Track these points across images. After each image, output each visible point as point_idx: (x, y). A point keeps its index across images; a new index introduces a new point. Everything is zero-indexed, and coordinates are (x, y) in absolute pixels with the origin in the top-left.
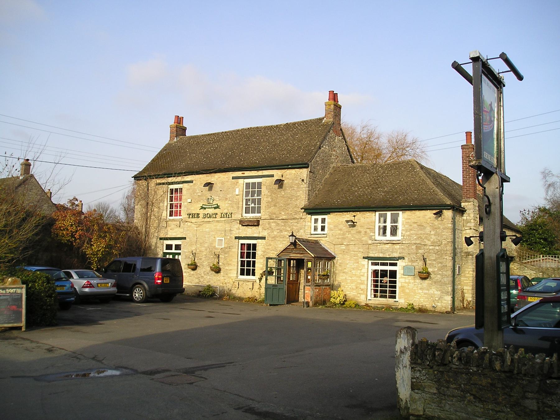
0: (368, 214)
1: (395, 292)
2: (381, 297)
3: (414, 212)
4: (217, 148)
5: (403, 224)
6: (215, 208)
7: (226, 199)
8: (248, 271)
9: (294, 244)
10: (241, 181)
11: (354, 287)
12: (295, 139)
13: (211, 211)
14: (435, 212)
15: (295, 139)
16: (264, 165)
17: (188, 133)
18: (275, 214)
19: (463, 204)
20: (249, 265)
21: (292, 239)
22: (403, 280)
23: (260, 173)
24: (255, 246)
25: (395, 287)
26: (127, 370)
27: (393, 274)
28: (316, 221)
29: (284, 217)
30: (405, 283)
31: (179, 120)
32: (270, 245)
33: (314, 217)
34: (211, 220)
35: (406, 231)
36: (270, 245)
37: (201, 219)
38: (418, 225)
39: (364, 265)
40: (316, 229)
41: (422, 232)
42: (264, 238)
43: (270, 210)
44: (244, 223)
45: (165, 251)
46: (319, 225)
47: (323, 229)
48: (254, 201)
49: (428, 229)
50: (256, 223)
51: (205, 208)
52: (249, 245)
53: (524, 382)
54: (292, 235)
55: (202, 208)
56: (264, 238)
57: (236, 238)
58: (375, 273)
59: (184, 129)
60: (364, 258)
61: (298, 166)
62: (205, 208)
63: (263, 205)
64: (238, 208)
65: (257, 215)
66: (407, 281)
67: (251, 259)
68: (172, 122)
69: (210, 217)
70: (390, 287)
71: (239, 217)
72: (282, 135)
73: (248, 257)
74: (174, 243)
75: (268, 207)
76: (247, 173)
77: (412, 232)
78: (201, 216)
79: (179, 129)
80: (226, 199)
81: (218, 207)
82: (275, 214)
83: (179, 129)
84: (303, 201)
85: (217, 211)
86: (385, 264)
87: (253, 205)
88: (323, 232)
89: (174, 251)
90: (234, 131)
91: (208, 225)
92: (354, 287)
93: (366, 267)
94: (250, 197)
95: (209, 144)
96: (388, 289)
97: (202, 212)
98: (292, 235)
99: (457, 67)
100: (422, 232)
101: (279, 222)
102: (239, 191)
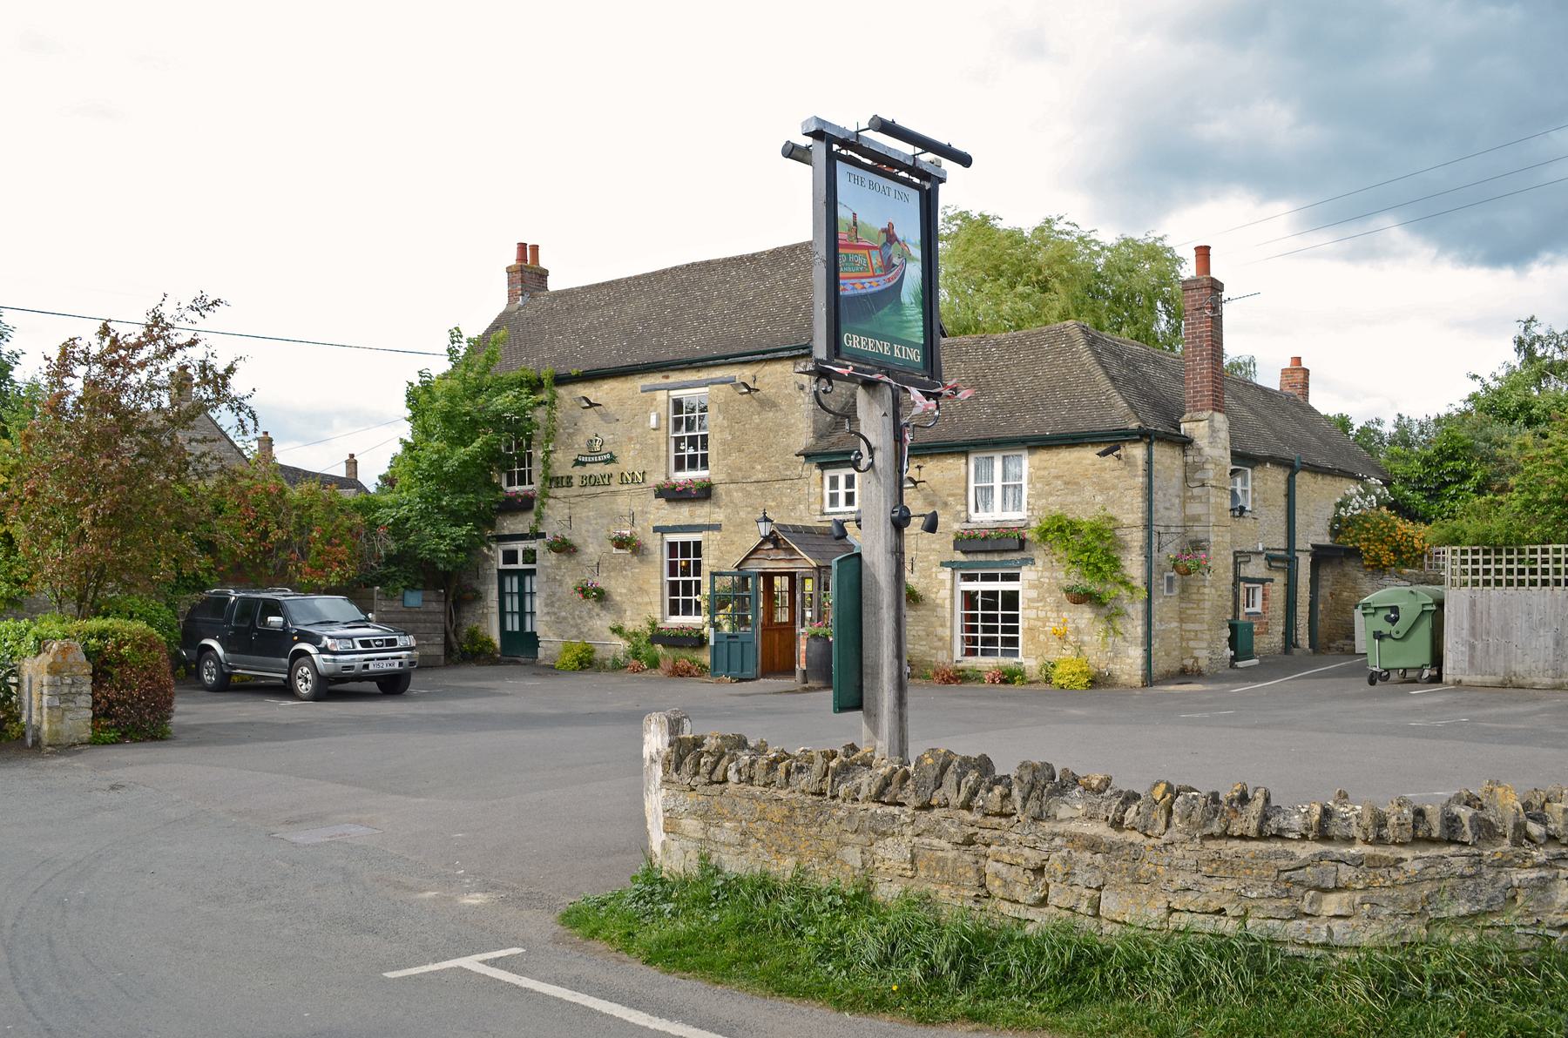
0: (950, 462)
1: (1015, 642)
2: (1004, 653)
3: (1055, 451)
4: (611, 317)
5: (1030, 482)
6: (606, 462)
7: (631, 439)
8: (687, 604)
9: (772, 539)
10: (661, 396)
11: (922, 633)
12: (788, 288)
13: (597, 470)
14: (1102, 449)
15: (788, 288)
16: (709, 355)
17: (554, 284)
18: (740, 469)
19: (1185, 427)
20: (687, 591)
21: (764, 529)
22: (1032, 614)
23: (704, 375)
24: (698, 545)
25: (1016, 630)
26: (293, 839)
27: (1011, 600)
28: (834, 482)
29: (760, 476)
30: (1038, 619)
31: (527, 252)
32: (733, 543)
33: (829, 473)
34: (599, 490)
35: (1039, 496)
36: (733, 543)
37: (575, 490)
38: (1066, 483)
39: (943, 582)
40: (834, 500)
41: (1075, 498)
42: (716, 527)
43: (729, 461)
44: (673, 495)
45: (502, 566)
46: (842, 490)
47: (850, 499)
48: (692, 441)
49: (1089, 491)
50: (704, 493)
51: (584, 464)
52: (685, 545)
53: (841, 813)
54: (766, 520)
55: (577, 463)
56: (716, 527)
57: (656, 529)
58: (969, 598)
59: (543, 275)
60: (942, 564)
61: (787, 354)
62: (584, 464)
63: (712, 452)
64: (658, 458)
65: (698, 474)
66: (1042, 614)
67: (692, 578)
68: (511, 259)
69: (596, 484)
70: (1005, 630)
71: (661, 479)
72: (763, 277)
73: (686, 572)
74: (519, 546)
75: (726, 453)
76: (676, 377)
77: (1051, 499)
78: (576, 481)
79: (528, 273)
80: (631, 439)
81: (612, 460)
82: (740, 469)
83: (528, 273)
84: (804, 438)
85: (609, 469)
86: (993, 578)
87: (691, 451)
88: (850, 508)
89: (520, 565)
90: (654, 274)
91: (592, 503)
92: (922, 633)
93: (948, 584)
94: (683, 433)
95: (596, 308)
96: (1000, 635)
97: (577, 472)
98: (766, 520)
99: (965, 160)
100: (1075, 498)
101: (751, 488)
102: (659, 418)
